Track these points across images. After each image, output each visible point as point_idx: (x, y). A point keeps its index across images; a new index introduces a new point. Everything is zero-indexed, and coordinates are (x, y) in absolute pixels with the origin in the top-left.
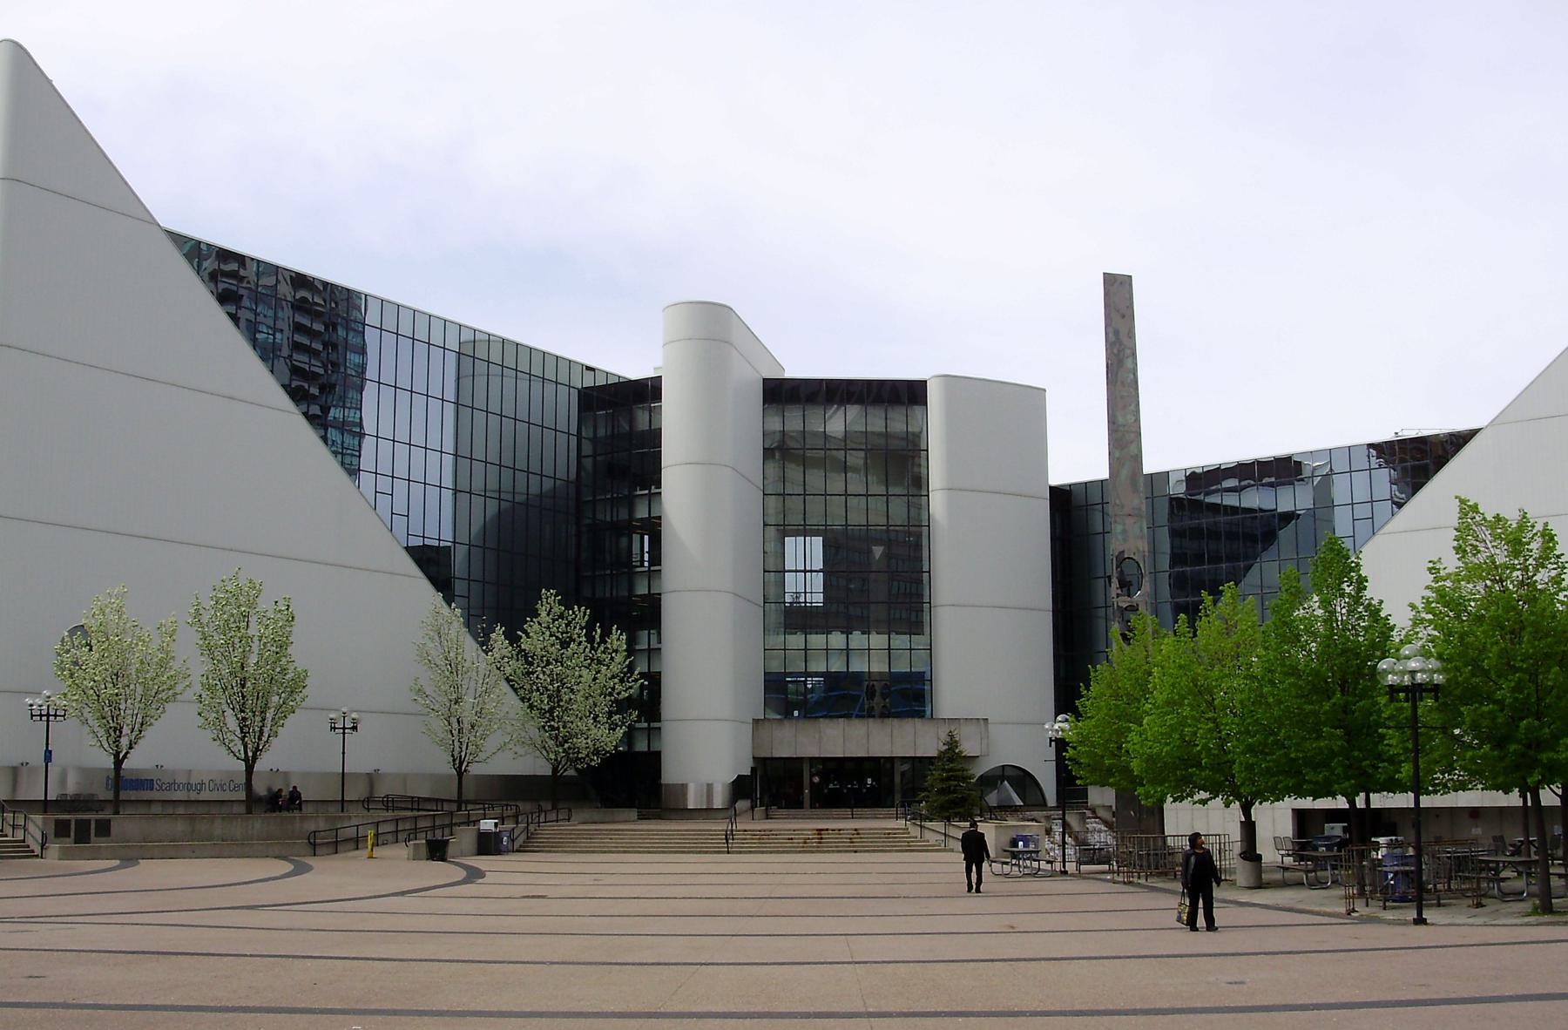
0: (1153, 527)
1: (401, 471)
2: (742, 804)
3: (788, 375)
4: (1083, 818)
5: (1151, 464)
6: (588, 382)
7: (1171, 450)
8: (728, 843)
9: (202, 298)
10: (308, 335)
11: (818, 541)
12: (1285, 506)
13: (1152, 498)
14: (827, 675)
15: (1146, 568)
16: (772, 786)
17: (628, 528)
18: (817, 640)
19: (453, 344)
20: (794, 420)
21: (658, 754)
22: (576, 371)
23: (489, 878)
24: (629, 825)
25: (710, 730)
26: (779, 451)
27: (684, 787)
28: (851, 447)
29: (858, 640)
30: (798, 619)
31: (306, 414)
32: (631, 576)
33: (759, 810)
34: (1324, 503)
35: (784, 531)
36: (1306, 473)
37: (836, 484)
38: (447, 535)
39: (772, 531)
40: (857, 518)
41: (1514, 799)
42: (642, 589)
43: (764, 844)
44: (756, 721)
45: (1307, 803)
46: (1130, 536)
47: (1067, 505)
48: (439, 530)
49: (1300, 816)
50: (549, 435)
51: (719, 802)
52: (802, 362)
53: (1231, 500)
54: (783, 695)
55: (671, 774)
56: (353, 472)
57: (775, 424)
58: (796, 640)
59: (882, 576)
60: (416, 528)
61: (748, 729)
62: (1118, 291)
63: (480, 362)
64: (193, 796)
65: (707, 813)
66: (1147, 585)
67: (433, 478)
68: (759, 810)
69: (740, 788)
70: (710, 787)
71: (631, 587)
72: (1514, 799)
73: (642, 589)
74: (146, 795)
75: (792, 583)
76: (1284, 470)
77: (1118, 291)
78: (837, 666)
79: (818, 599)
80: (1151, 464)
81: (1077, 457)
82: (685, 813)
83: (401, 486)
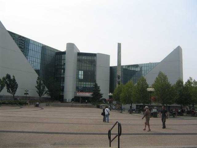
0: (122, 72)
1: (35, 61)
2: (73, 102)
3: (80, 52)
4: (112, 105)
5: (122, 65)
6: (57, 51)
7: (124, 63)
8: (72, 106)
9: (8, 33)
10: (23, 43)
11: (83, 72)
12: (137, 70)
13: (122, 69)
14: (83, 87)
15: (121, 76)
16: (77, 100)
17: (61, 69)
18: (82, 83)
19: (41, 46)
20: (81, 57)
21: (63, 95)
22: (56, 50)
23: (44, 109)
24: (59, 103)
25: (69, 92)
26: (79, 61)
27: (66, 99)
28: (88, 61)
29: (87, 83)
30: (80, 80)
31: (21, 50)
32: (61, 74)
33: (75, 103)
34: (141, 70)
35: (79, 70)
36: (139, 66)
37: (85, 65)
38: (40, 69)
39: (78, 70)
40: (88, 69)
41: (180, 105)
42: (62, 85)
43: (75, 106)
44: (75, 92)
45: (137, 104)
46: (119, 73)
47: (112, 69)
48: (39, 68)
49: (137, 106)
50: (53, 52)
51: (70, 101)
52: (82, 51)
53: (131, 69)
54: (78, 89)
55: (65, 98)
56: (27, 59)
57: (79, 58)
58: (80, 83)
59: (90, 76)
60: (36, 68)
61: (74, 93)
62: (119, 45)
63: (44, 48)
64: (7, 98)
65: (69, 102)
66: (121, 79)
67: (38, 62)
68: (75, 103)
69: (73, 100)
70: (69, 99)
71: (61, 76)
72: (180, 105)
73: (62, 85)
74: (2, 98)
75: (80, 76)
76: (136, 66)
77: (119, 45)
78: (85, 86)
79: (82, 78)
80: (122, 65)
81: (113, 63)
82: (66, 102)
83: (34, 63)
